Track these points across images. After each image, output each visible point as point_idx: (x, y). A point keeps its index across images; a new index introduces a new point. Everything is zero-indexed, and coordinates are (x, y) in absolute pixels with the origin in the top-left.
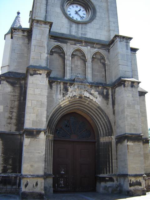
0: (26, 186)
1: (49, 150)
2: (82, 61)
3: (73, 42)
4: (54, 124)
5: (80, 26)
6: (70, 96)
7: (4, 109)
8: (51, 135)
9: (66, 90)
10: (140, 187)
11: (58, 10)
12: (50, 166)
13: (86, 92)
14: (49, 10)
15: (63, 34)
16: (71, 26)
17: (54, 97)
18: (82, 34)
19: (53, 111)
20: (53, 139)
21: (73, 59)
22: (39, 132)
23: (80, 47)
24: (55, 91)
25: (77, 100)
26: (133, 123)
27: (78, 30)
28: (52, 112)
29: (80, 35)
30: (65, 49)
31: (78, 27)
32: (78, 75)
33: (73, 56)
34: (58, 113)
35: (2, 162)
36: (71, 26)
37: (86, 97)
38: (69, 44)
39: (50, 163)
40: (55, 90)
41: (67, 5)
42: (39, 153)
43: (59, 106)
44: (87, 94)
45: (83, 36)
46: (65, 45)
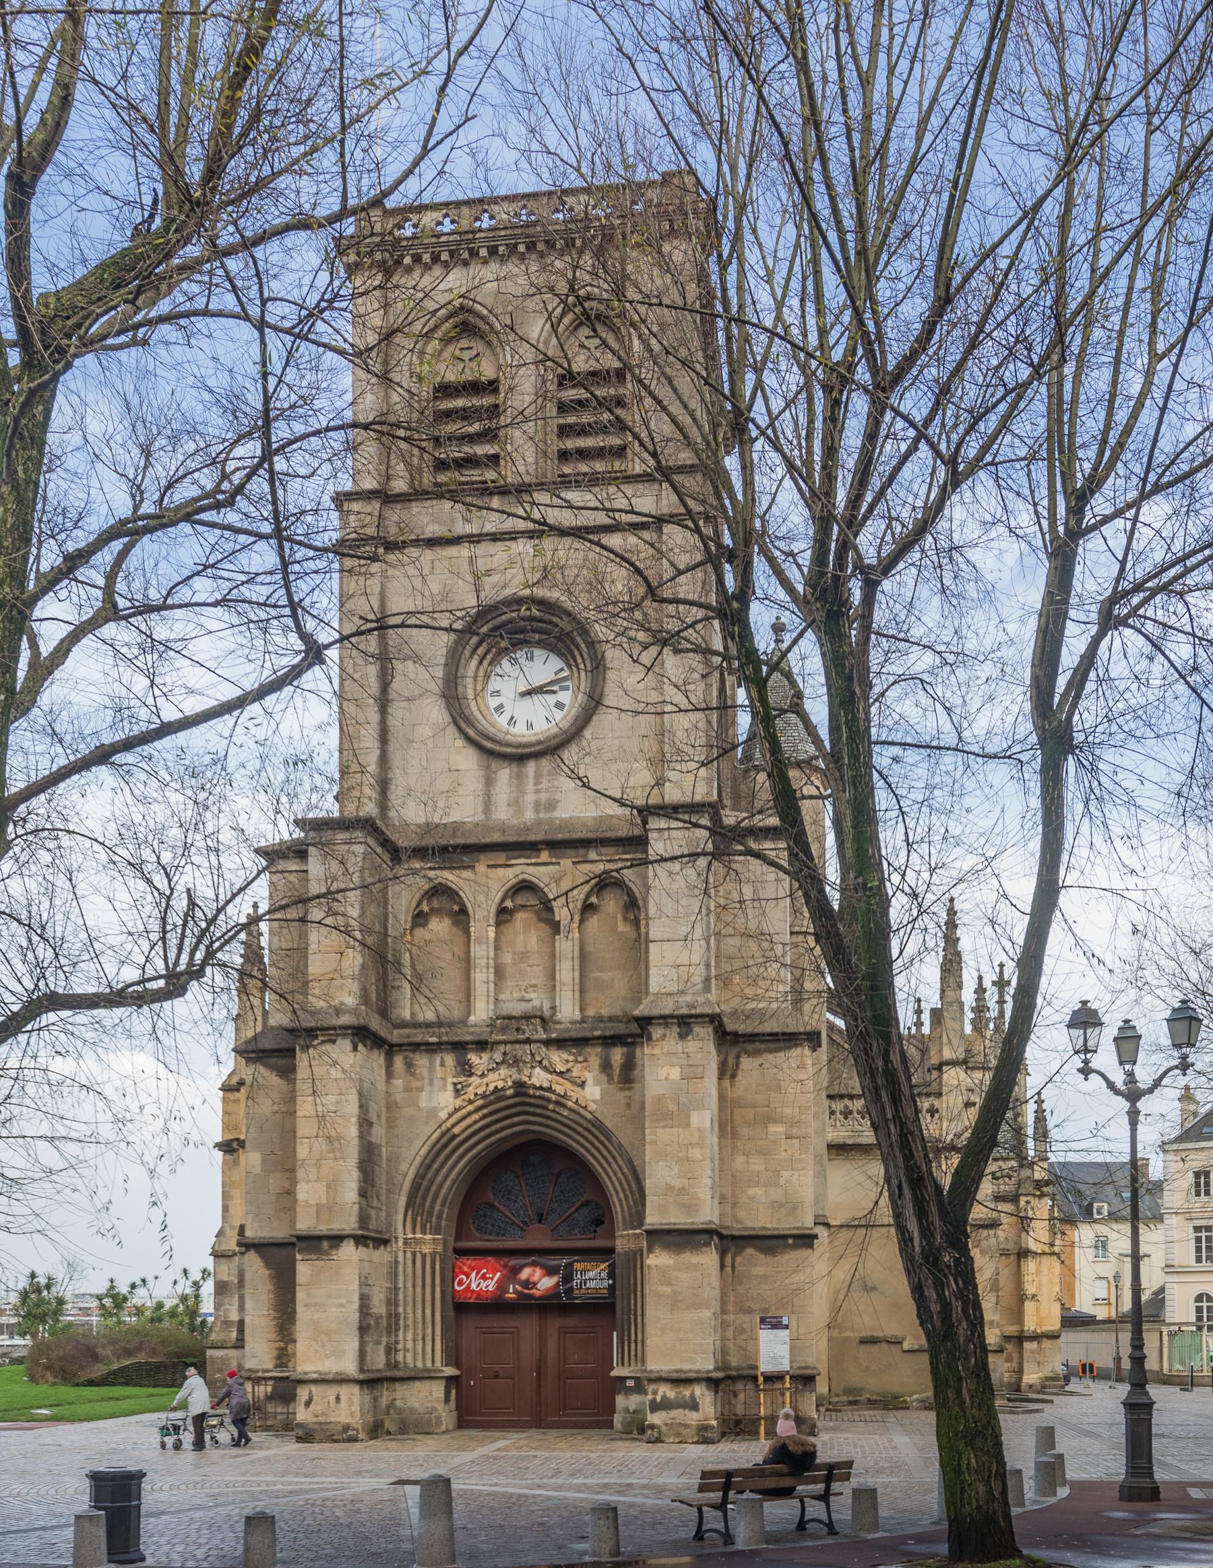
0: (308, 1404)
1: (419, 1290)
2: (545, 930)
3: (500, 858)
4: (442, 1194)
5: (531, 767)
6: (480, 1091)
7: (264, 1161)
8: (429, 1237)
9: (466, 1069)
10: (694, 1415)
11: (434, 712)
12: (429, 1338)
13: (538, 1070)
14: (394, 722)
15: (456, 827)
16: (489, 782)
17: (423, 1104)
18: (537, 806)
19: (423, 1152)
20: (440, 1249)
21: (508, 930)
22: (337, 1239)
23: (531, 869)
24: (426, 1081)
25: (511, 1101)
26: (677, 1183)
27: (522, 792)
28: (418, 1159)
29: (529, 815)
30: (467, 895)
31: (520, 778)
32: (528, 996)
33: (503, 915)
34: (592, 1144)
35: (273, 1336)
36: (489, 782)
37: (541, 1088)
38: (481, 868)
39: (429, 1331)
40: (425, 1073)
41: (480, 663)
42: (342, 1305)
43: (443, 1134)
44: (539, 1077)
45: (542, 815)
46: (466, 874)
